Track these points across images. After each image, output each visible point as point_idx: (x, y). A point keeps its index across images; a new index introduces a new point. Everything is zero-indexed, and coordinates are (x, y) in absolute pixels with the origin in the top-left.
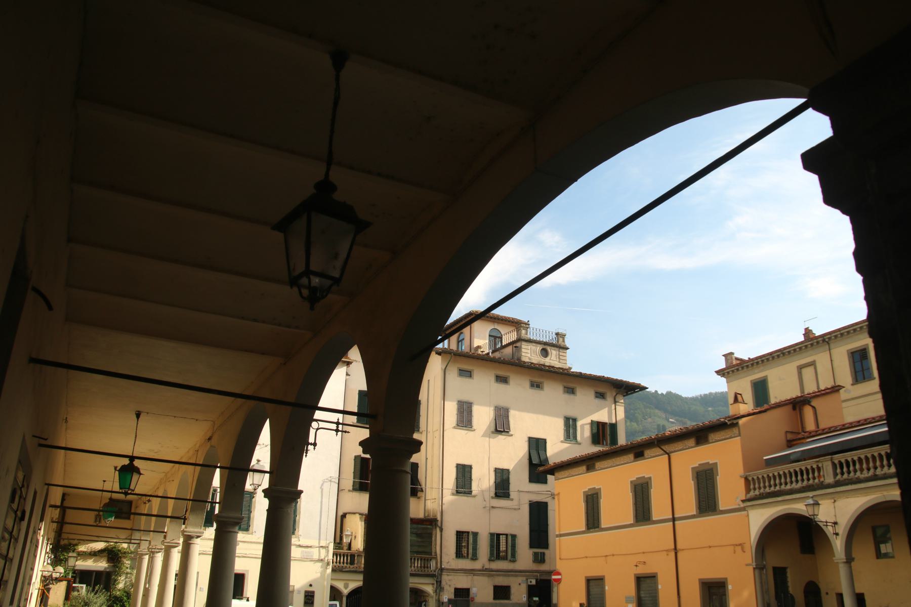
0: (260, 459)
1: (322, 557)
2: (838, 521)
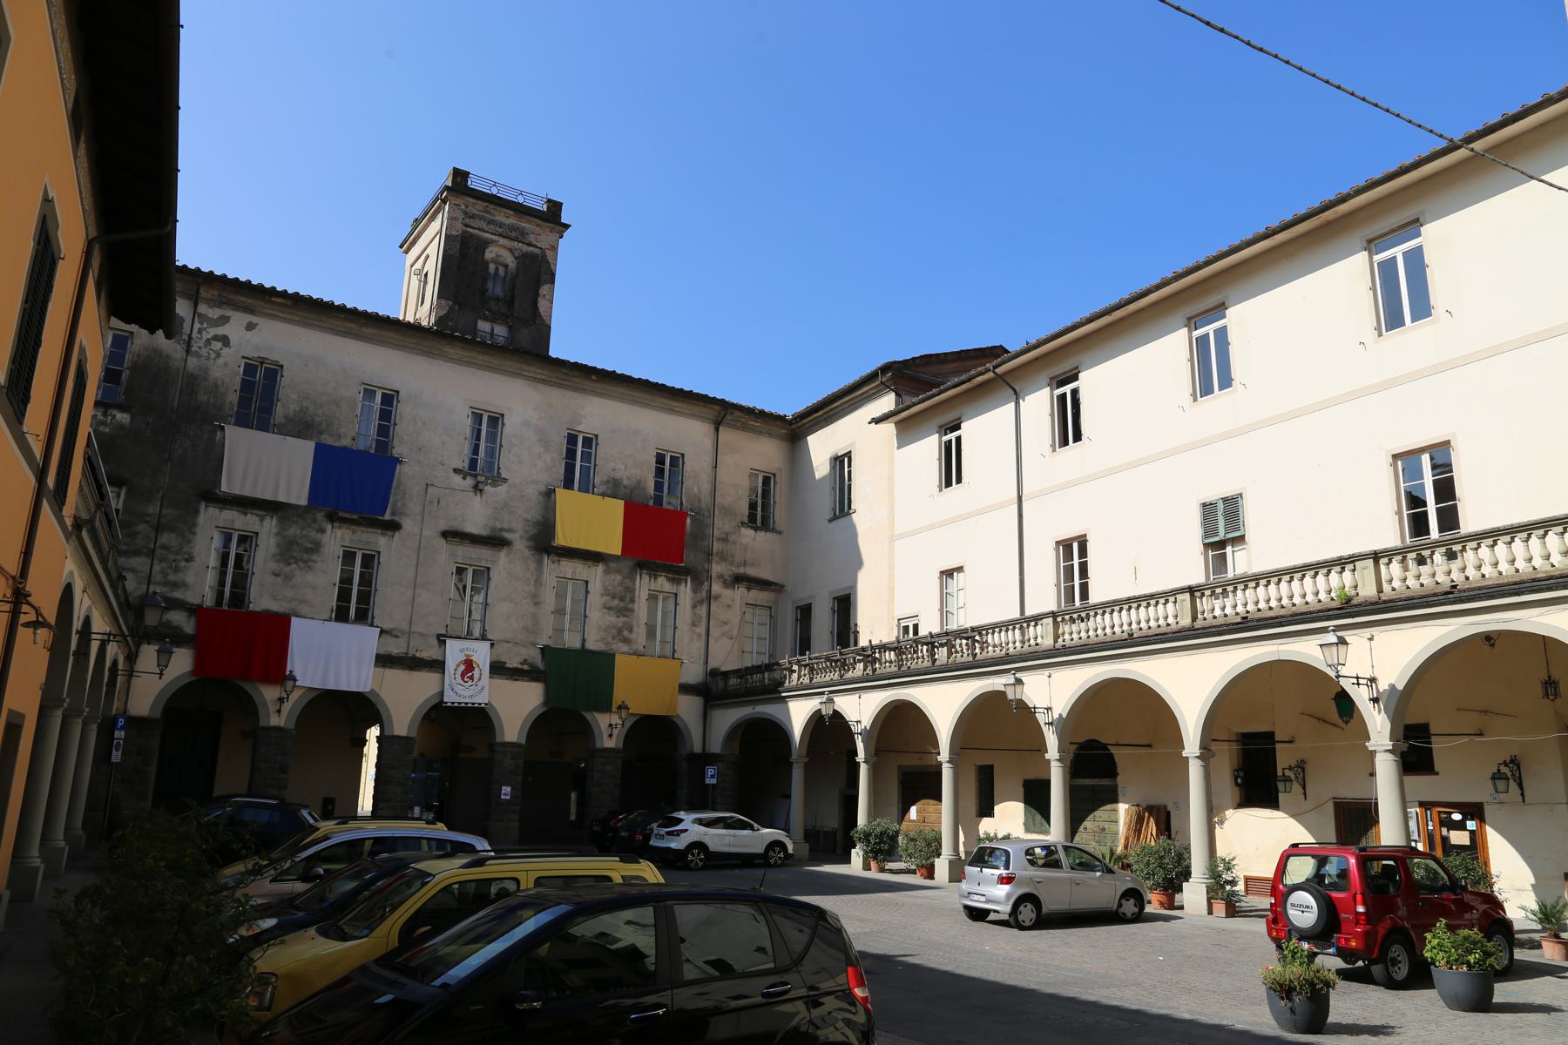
0: (1563, 689)
2: (1377, 675)
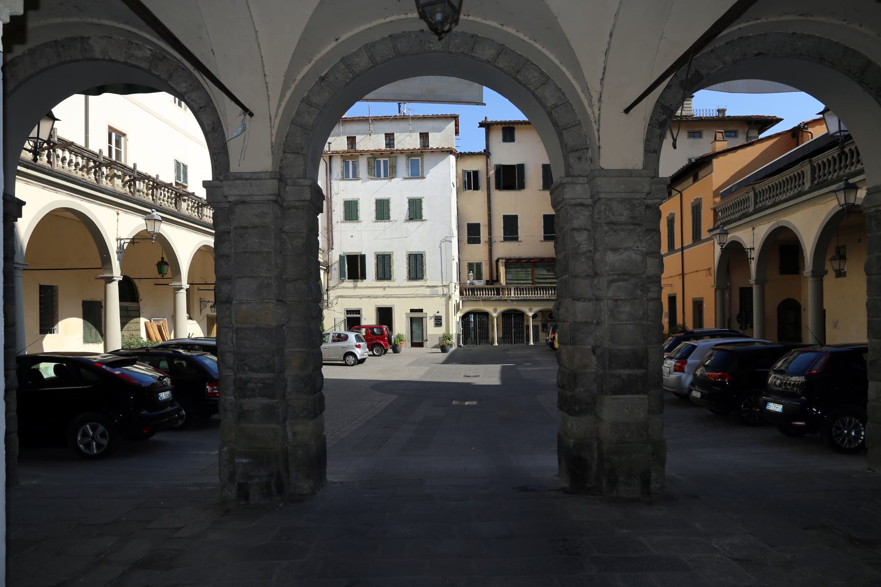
1: (445, 293)
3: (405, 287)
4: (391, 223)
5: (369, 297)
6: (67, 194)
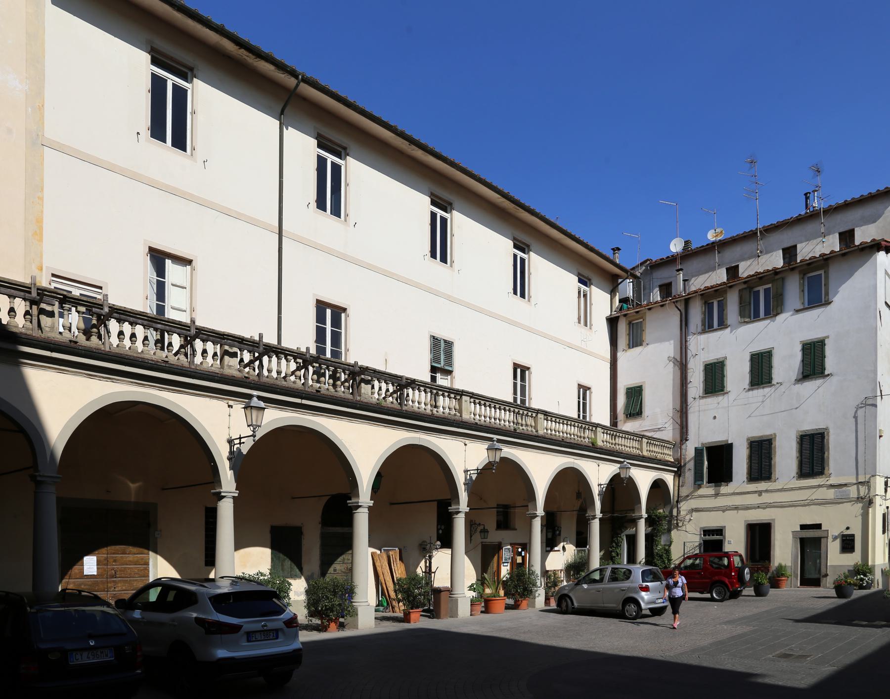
1: (862, 494)
3: (792, 489)
4: (773, 389)
5: (736, 508)
6: (132, 382)
